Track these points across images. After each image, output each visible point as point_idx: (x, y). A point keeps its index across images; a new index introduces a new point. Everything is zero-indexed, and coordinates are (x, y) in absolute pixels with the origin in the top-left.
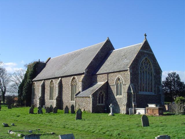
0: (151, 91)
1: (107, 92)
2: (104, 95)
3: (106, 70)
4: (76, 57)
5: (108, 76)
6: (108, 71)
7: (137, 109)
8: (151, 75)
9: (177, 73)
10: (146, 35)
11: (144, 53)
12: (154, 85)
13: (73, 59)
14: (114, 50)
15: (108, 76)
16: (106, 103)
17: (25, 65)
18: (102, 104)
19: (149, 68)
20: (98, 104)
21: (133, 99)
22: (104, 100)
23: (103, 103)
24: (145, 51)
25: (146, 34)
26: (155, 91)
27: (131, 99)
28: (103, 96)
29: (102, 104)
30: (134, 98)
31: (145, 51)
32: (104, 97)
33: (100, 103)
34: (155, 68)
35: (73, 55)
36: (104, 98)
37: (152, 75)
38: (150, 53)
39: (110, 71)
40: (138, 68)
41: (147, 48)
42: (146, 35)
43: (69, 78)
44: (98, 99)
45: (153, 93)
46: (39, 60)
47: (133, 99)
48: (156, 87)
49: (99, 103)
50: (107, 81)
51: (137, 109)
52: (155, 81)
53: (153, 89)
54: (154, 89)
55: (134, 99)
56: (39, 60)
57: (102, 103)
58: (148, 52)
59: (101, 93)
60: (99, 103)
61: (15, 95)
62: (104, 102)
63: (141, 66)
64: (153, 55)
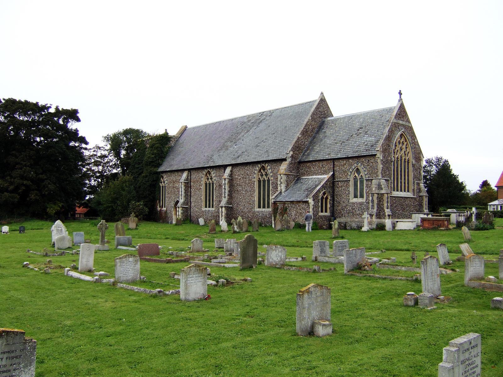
0: (408, 191)
1: (333, 192)
2: (329, 197)
3: (329, 154)
4: (253, 126)
5: (334, 164)
6: (333, 156)
7: (397, 222)
8: (408, 162)
9: (445, 158)
10: (400, 93)
12: (412, 181)
13: (248, 131)
14: (329, 119)
15: (334, 164)
17: (105, 137)
19: (405, 152)
20: (321, 214)
22: (329, 206)
23: (327, 212)
25: (400, 91)
26: (413, 190)
27: (383, 205)
28: (327, 198)
29: (324, 214)
31: (401, 122)
32: (328, 200)
33: (265, 208)
34: (413, 150)
35: (245, 123)
36: (328, 203)
37: (410, 163)
38: (407, 124)
39: (339, 156)
41: (403, 117)
42: (400, 93)
43: (250, 167)
45: (409, 195)
46: (166, 130)
47: (385, 205)
48: (416, 184)
50: (332, 173)
51: (397, 222)
52: (414, 174)
53: (411, 187)
54: (412, 188)
56: (166, 130)
57: (326, 211)
58: (404, 123)
59: (324, 194)
60: (259, 207)
61: (467, 229)
64: (411, 128)
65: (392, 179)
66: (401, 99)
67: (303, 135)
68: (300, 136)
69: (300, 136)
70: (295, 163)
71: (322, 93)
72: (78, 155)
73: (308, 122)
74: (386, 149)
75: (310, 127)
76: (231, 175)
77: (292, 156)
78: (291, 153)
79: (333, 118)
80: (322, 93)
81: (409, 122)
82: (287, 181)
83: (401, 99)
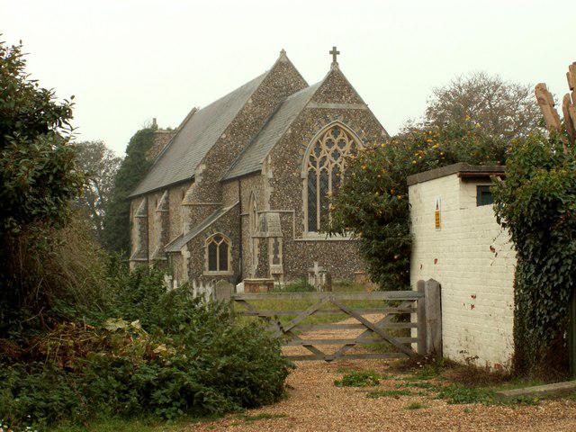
2: (230, 244)
5: (240, 186)
10: (335, 53)
11: (324, 112)
15: (240, 186)
16: (235, 268)
18: (223, 273)
21: (272, 257)
22: (230, 258)
23: (226, 269)
24: (332, 106)
25: (334, 48)
28: (224, 246)
30: (276, 252)
31: (332, 106)
32: (229, 249)
33: (216, 269)
38: (353, 107)
40: (298, 161)
41: (339, 94)
42: (335, 53)
44: (206, 257)
46: (155, 120)
47: (272, 257)
49: (212, 267)
55: (276, 257)
56: (155, 120)
57: (224, 267)
59: (218, 238)
60: (212, 267)
62: (229, 266)
63: (314, 155)
64: (367, 113)
65: (305, 208)
66: (335, 63)
67: (232, 133)
68: (224, 136)
69: (224, 136)
70: (211, 185)
71: (283, 53)
72: (61, 174)
73: (243, 109)
74: (283, 160)
75: (251, 118)
76: (166, 205)
77: (205, 173)
78: (204, 167)
79: (308, 88)
80: (283, 53)
81: (360, 101)
82: (192, 217)
83: (335, 63)
